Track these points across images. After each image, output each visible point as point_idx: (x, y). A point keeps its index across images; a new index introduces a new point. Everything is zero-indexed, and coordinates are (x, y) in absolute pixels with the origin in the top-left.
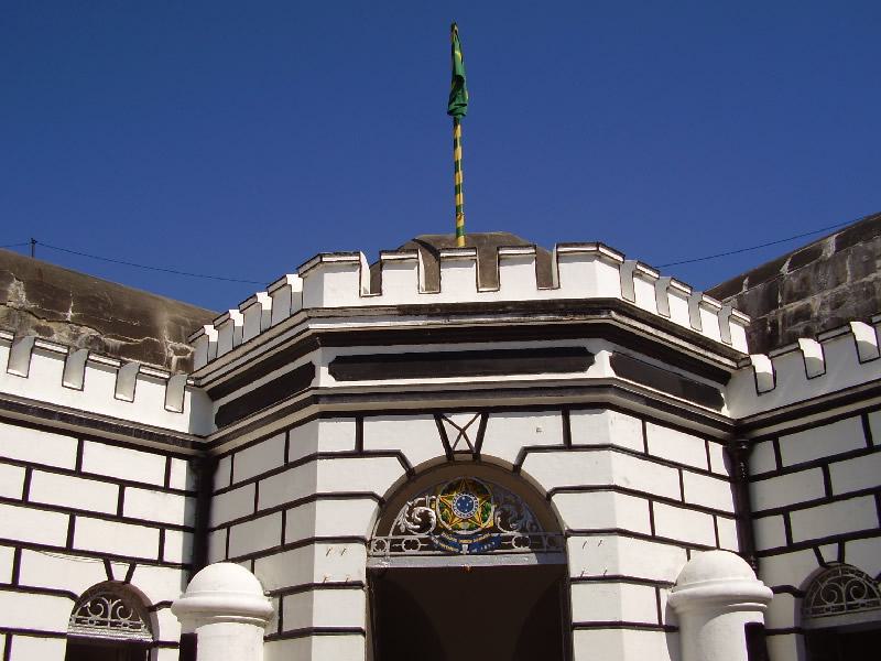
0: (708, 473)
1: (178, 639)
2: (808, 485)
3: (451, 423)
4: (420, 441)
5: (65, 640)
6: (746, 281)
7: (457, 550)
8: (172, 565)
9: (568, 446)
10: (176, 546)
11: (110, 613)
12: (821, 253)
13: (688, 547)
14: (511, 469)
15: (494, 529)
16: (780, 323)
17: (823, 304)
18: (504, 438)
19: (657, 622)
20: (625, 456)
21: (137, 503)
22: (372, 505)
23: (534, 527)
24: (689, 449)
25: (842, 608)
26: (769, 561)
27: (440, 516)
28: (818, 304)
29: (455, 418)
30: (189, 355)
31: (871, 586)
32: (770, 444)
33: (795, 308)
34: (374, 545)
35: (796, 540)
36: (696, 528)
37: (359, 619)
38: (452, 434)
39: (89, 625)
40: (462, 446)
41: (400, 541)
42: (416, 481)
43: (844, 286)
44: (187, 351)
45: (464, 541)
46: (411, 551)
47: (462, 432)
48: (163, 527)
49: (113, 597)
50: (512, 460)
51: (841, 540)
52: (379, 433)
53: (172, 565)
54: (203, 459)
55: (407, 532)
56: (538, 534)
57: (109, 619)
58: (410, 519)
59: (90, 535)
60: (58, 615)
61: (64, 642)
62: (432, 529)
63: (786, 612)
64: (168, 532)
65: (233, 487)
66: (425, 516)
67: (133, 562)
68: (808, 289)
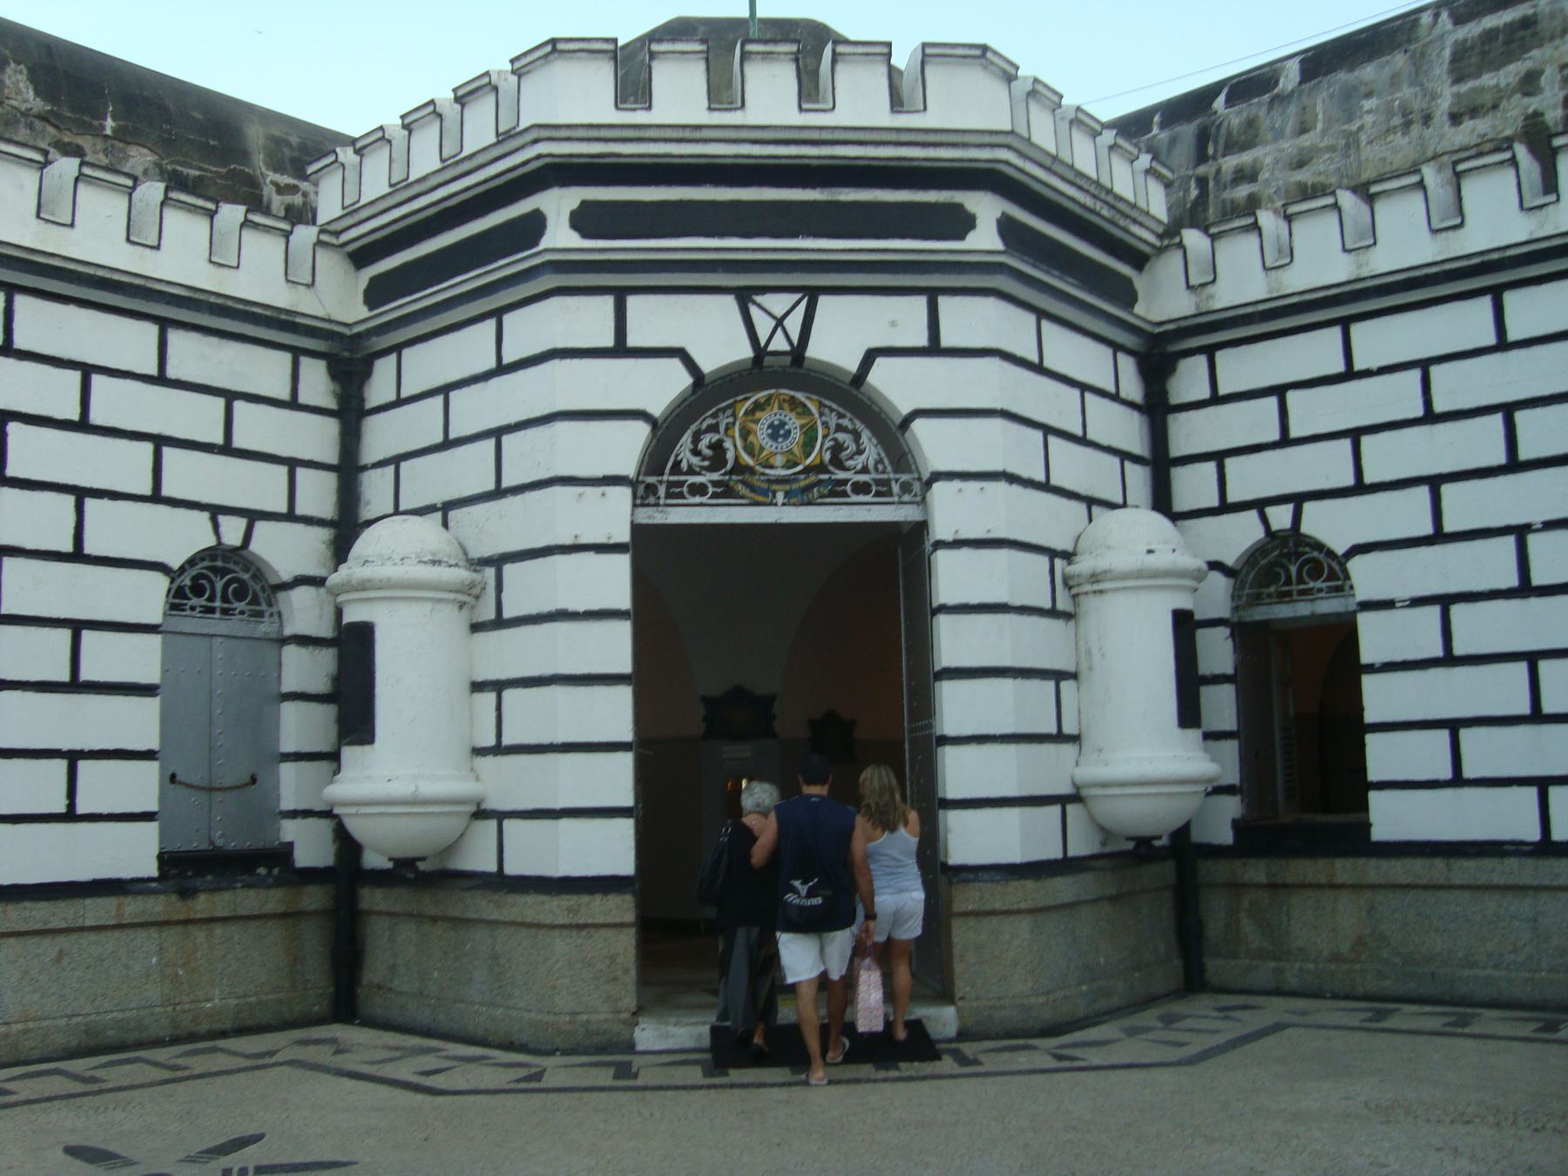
0: (1115, 397)
3: (760, 306)
4: (715, 333)
6: (1157, 119)
8: (309, 521)
9: (934, 348)
10: (318, 493)
11: (219, 595)
12: (1277, 83)
13: (1091, 502)
14: (848, 379)
15: (820, 468)
17: (1277, 161)
18: (842, 332)
20: (105, 810)
21: (253, 427)
22: (641, 430)
23: (880, 467)
29: (766, 300)
34: (641, 489)
37: (620, 595)
38: (763, 326)
40: (779, 344)
41: (681, 484)
42: (709, 393)
47: (780, 322)
48: (292, 464)
50: (852, 365)
51: (1298, 500)
52: (652, 319)
53: (309, 521)
54: (349, 358)
55: (691, 471)
56: (885, 476)
57: (218, 604)
58: (696, 452)
59: (188, 474)
60: (146, 597)
62: (729, 466)
63: (1216, 597)
64: (301, 473)
65: (399, 402)
66: (717, 447)
67: (253, 517)
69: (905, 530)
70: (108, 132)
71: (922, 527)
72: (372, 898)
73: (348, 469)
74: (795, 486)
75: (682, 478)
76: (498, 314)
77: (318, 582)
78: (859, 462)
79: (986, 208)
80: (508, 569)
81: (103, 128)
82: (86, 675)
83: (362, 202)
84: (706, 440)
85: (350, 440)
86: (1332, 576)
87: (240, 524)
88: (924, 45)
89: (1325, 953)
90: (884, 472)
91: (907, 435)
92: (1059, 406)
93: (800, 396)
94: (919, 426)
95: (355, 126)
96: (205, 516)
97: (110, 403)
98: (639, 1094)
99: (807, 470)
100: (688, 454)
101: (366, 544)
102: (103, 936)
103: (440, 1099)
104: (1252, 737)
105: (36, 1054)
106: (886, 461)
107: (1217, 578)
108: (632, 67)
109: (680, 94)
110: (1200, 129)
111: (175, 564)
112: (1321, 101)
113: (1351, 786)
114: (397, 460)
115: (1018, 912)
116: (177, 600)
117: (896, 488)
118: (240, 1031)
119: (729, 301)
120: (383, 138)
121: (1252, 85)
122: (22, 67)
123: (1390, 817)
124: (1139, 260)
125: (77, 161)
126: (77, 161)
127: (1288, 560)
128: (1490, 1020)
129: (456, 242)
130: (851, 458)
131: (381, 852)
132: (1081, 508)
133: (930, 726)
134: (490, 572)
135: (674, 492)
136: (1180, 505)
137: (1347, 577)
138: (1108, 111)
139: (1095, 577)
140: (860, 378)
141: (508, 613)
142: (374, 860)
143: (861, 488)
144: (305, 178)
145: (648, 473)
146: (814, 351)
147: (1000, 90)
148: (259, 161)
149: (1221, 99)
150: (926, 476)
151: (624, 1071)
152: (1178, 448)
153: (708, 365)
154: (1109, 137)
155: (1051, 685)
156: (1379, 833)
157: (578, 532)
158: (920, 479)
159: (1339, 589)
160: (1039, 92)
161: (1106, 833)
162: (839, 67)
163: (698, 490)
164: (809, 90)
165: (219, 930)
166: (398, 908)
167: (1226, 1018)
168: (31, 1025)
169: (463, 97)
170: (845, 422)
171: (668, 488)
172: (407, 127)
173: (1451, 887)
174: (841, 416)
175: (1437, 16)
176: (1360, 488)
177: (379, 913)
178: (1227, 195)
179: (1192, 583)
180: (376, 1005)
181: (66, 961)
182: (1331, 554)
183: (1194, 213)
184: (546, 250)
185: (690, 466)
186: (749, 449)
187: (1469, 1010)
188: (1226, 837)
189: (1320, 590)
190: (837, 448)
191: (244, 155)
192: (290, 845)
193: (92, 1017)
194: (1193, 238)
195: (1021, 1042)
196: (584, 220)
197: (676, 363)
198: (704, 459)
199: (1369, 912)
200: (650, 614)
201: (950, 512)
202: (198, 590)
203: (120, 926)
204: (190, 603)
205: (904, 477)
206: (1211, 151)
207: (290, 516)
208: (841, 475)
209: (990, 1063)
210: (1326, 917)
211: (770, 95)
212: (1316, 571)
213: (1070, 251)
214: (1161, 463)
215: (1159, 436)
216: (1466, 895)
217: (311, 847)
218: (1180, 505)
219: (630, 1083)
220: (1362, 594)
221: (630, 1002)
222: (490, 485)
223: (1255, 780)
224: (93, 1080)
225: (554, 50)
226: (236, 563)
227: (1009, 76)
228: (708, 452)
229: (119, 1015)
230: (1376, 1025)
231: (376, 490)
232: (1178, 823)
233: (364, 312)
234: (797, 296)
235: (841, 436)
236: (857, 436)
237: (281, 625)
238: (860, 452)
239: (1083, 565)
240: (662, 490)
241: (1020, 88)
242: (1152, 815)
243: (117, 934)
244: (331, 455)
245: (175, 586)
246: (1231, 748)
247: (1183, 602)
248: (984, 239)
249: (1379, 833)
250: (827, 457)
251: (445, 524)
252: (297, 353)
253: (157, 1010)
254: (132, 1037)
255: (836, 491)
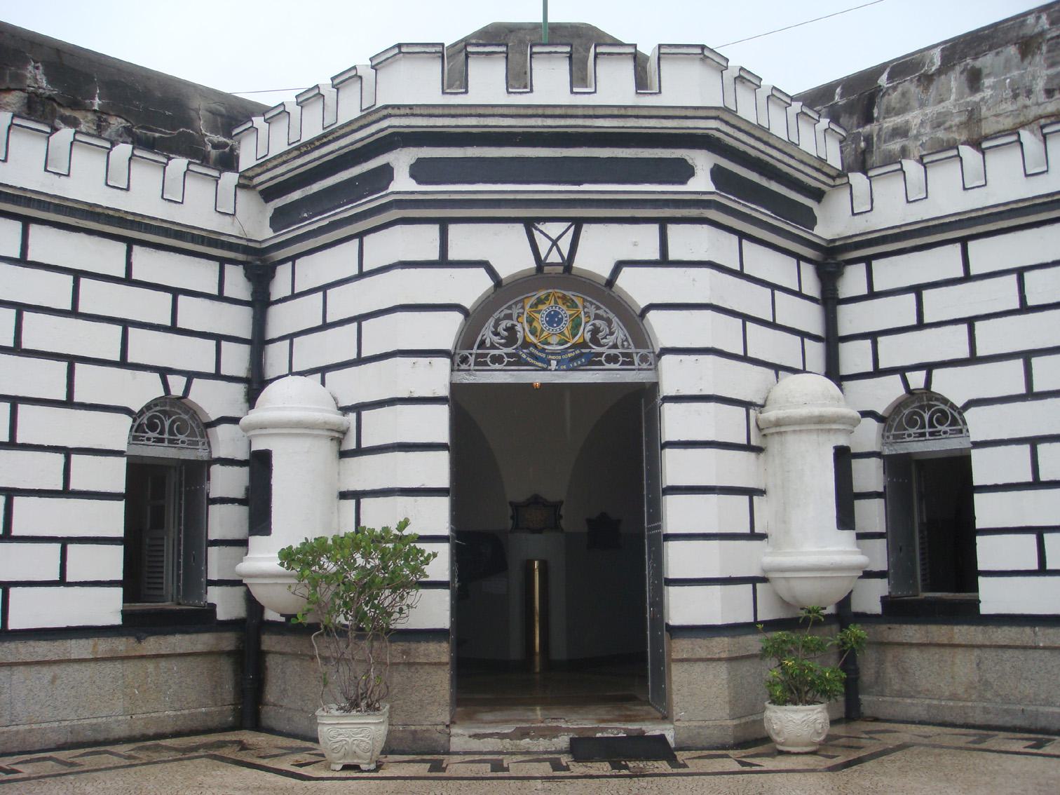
0: (798, 294)
1: (444, 391)
2: (901, 310)
3: (541, 232)
4: (510, 251)
5: (125, 458)
6: (838, 90)
7: (545, 366)
9: (664, 261)
10: (236, 360)
11: (167, 430)
13: (777, 368)
14: (604, 282)
15: (584, 345)
16: (875, 139)
17: (922, 123)
18: (598, 251)
19: (745, 442)
20: (1005, 437)
21: (193, 314)
23: (625, 343)
24: (777, 268)
25: (923, 435)
26: (846, 384)
27: (527, 330)
28: (918, 121)
29: (544, 227)
30: (227, 150)
31: (956, 414)
32: (862, 267)
33: (891, 124)
34: (457, 359)
35: (882, 365)
36: (782, 348)
39: (146, 442)
40: (555, 258)
41: (485, 355)
42: (504, 291)
43: (946, 104)
44: (226, 145)
45: (553, 357)
46: (497, 366)
47: (555, 243)
48: (218, 338)
49: (168, 416)
50: (606, 273)
51: (929, 367)
52: (465, 241)
55: (493, 347)
57: (166, 436)
58: (496, 334)
59: (144, 347)
60: (117, 432)
61: (124, 461)
62: (519, 342)
65: (294, 296)
66: (512, 330)
67: (191, 376)
68: (908, 104)
69: (647, 386)
70: (96, 108)
71: (655, 386)
72: (269, 642)
73: (258, 343)
74: (564, 357)
75: (487, 351)
76: (360, 235)
77: (235, 421)
78: (610, 340)
79: (703, 162)
80: (365, 414)
81: (92, 104)
82: (74, 485)
83: (339, 124)
84: (504, 324)
85: (260, 323)
86: (954, 422)
87: (183, 380)
88: (660, 46)
89: (947, 694)
90: (628, 348)
91: (644, 321)
92: (755, 301)
93: (569, 294)
94: (652, 316)
95: (270, 101)
96: (156, 376)
97: (95, 297)
98: (444, 782)
99: (575, 346)
100: (491, 335)
101: (270, 393)
102: (82, 667)
103: (306, 783)
104: (896, 535)
105: (37, 747)
106: (630, 340)
107: (871, 423)
108: (455, 59)
109: (487, 84)
110: (855, 102)
111: (136, 409)
112: (954, 81)
113: (964, 573)
114: (291, 337)
115: (720, 659)
116: (137, 433)
117: (636, 360)
118: (177, 734)
119: (520, 228)
120: (356, 75)
121: (903, 68)
122: (39, 64)
123: (994, 596)
124: (818, 195)
125: (73, 131)
126: (73, 131)
127: (923, 408)
128: (999, 741)
129: (333, 182)
130: (605, 338)
131: (276, 610)
132: (771, 373)
133: (659, 527)
134: (352, 417)
135: (481, 362)
136: (845, 370)
137: (964, 423)
138: (796, 86)
139: (778, 423)
140: (610, 282)
141: (365, 444)
142: (271, 615)
143: (612, 359)
144: (231, 137)
145: (463, 348)
146: (580, 263)
147: (714, 78)
148: (202, 126)
149: (885, 76)
150: (657, 351)
151: (437, 766)
152: (845, 329)
153: (504, 273)
154: (797, 107)
155: (746, 498)
156: (985, 609)
157: (412, 390)
158: (654, 352)
159: (961, 431)
160: (745, 78)
161: (785, 603)
162: (598, 62)
163: (497, 359)
164: (579, 77)
165: (163, 664)
166: (288, 650)
167: (871, 738)
168: (34, 726)
169: (339, 83)
170: (600, 312)
171: (476, 358)
172: (337, 87)
173: (1036, 648)
174: (598, 308)
175: (1038, 18)
176: (973, 359)
177: (276, 653)
178: (885, 147)
179: (850, 428)
180: (270, 715)
181: (58, 682)
182: (953, 406)
183: (861, 162)
184: (393, 193)
185: (492, 343)
186: (533, 332)
187: (1046, 737)
188: (877, 608)
189: (945, 433)
190: (595, 331)
191: (189, 123)
192: (213, 606)
193: (75, 722)
194: (857, 179)
195: (720, 752)
196: (420, 171)
197: (482, 271)
198: (502, 338)
199: (978, 665)
200: (467, 444)
201: (674, 376)
202: (152, 427)
203: (96, 660)
204: (147, 435)
205: (643, 351)
206: (876, 113)
207: (217, 376)
208: (597, 349)
209: (693, 767)
210: (935, 669)
211: (551, 84)
212: (943, 417)
213: (763, 191)
214: (832, 340)
215: (831, 320)
216: (1047, 653)
217: (226, 605)
218: (845, 370)
219: (440, 774)
220: (976, 436)
221: (446, 718)
222: (354, 356)
223: (896, 571)
224: (72, 764)
225: (400, 52)
226: (180, 408)
227: (720, 64)
228: (506, 333)
229: (94, 721)
230: (976, 746)
231: (276, 357)
232: (840, 596)
233: (269, 233)
234: (566, 225)
235: (598, 322)
236: (609, 322)
237: (210, 452)
238: (611, 333)
239: (771, 414)
240: (472, 360)
241: (729, 75)
242: (824, 595)
243: (92, 664)
244: (246, 332)
245: (136, 424)
246: (881, 544)
247: (842, 441)
248: (701, 183)
249: (985, 609)
250: (588, 336)
251: (323, 383)
252: (223, 262)
253: (120, 718)
254: (101, 737)
255: (592, 361)
